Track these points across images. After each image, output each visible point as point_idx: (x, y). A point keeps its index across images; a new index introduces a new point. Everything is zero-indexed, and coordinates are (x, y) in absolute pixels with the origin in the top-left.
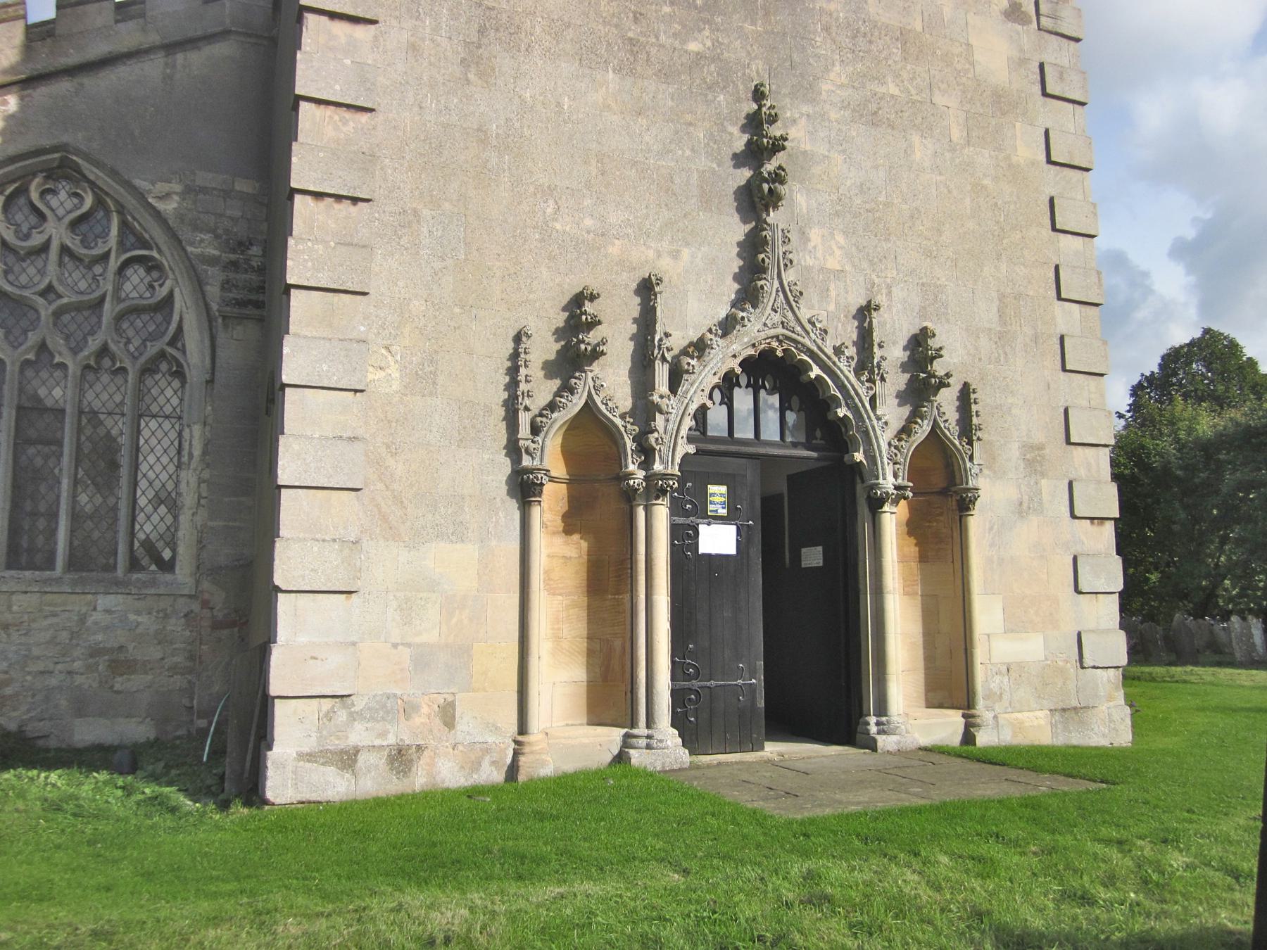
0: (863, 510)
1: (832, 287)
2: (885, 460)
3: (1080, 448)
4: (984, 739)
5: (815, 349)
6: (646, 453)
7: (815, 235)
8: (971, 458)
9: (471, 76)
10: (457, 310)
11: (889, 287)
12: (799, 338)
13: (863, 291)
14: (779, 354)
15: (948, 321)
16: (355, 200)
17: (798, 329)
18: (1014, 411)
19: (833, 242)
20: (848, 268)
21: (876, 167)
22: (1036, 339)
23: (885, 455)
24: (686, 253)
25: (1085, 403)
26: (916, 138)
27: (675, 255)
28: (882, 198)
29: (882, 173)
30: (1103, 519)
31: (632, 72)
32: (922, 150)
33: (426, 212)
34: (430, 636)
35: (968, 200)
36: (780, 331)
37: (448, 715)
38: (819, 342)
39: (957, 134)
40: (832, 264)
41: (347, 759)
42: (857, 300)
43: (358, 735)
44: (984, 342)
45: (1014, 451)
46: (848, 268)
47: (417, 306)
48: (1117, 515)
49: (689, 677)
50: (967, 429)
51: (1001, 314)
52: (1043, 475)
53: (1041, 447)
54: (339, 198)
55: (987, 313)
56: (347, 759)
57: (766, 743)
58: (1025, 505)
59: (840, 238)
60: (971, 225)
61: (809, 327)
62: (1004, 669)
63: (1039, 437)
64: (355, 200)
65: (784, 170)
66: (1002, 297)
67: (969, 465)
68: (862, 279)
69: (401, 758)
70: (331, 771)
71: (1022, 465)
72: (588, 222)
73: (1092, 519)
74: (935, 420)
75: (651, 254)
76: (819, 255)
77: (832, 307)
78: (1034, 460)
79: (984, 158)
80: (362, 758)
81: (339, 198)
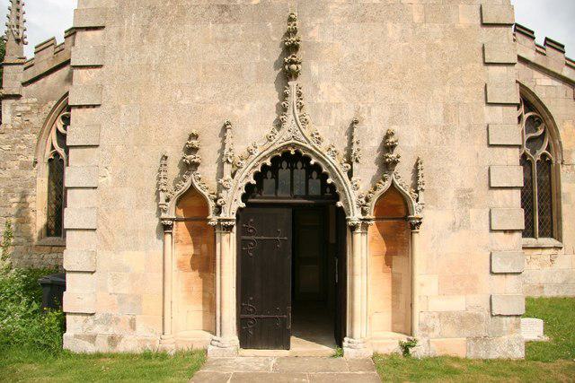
0: (348, 231)
1: (333, 112)
2: (355, 206)
3: (499, 191)
4: (419, 351)
5: (313, 149)
6: (219, 210)
7: (323, 86)
8: (417, 200)
9: (144, 41)
10: (135, 147)
11: (369, 108)
12: (304, 144)
13: (353, 113)
14: (293, 153)
15: (408, 124)
16: (94, 106)
17: (303, 139)
18: (452, 171)
19: (334, 89)
20: (343, 101)
21: (364, 44)
22: (469, 128)
23: (355, 203)
24: (248, 107)
25: (505, 163)
26: (390, 25)
27: (242, 107)
28: (367, 60)
29: (366, 47)
30: (512, 231)
31: (221, 22)
32: (393, 30)
33: (123, 106)
34: (125, 291)
35: (424, 54)
36: (292, 141)
37: (133, 325)
38: (316, 145)
39: (417, 18)
40: (333, 100)
41: (92, 339)
42: (348, 117)
43: (98, 329)
44: (432, 134)
45: (451, 194)
46: (343, 101)
47: (119, 148)
48: (523, 228)
49: (248, 312)
50: (415, 186)
51: (445, 116)
52: (471, 206)
53: (470, 191)
54: (88, 106)
55: (435, 116)
56: (92, 339)
57: (293, 338)
58: (457, 224)
59: (339, 86)
60: (426, 67)
61: (309, 138)
62: (436, 315)
63: (468, 185)
64: (94, 106)
65: (559, 48)
66: (446, 107)
67: (415, 204)
68: (352, 106)
69: (113, 340)
70: (87, 343)
71: (456, 201)
72: (197, 98)
73: (505, 231)
74: (393, 181)
75: (229, 109)
76: (325, 97)
77: (333, 124)
78: (465, 198)
79: (436, 30)
80: (98, 339)
81: (88, 106)
